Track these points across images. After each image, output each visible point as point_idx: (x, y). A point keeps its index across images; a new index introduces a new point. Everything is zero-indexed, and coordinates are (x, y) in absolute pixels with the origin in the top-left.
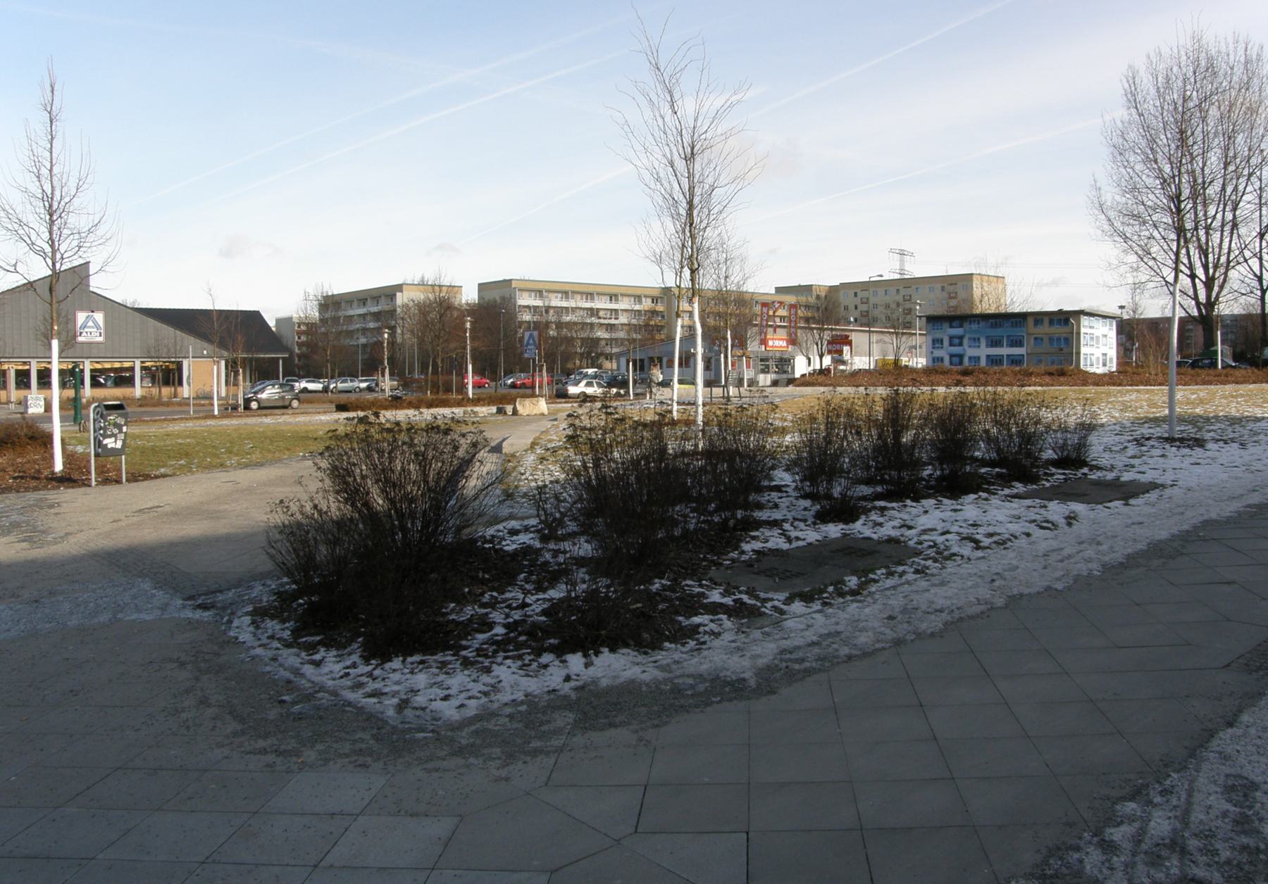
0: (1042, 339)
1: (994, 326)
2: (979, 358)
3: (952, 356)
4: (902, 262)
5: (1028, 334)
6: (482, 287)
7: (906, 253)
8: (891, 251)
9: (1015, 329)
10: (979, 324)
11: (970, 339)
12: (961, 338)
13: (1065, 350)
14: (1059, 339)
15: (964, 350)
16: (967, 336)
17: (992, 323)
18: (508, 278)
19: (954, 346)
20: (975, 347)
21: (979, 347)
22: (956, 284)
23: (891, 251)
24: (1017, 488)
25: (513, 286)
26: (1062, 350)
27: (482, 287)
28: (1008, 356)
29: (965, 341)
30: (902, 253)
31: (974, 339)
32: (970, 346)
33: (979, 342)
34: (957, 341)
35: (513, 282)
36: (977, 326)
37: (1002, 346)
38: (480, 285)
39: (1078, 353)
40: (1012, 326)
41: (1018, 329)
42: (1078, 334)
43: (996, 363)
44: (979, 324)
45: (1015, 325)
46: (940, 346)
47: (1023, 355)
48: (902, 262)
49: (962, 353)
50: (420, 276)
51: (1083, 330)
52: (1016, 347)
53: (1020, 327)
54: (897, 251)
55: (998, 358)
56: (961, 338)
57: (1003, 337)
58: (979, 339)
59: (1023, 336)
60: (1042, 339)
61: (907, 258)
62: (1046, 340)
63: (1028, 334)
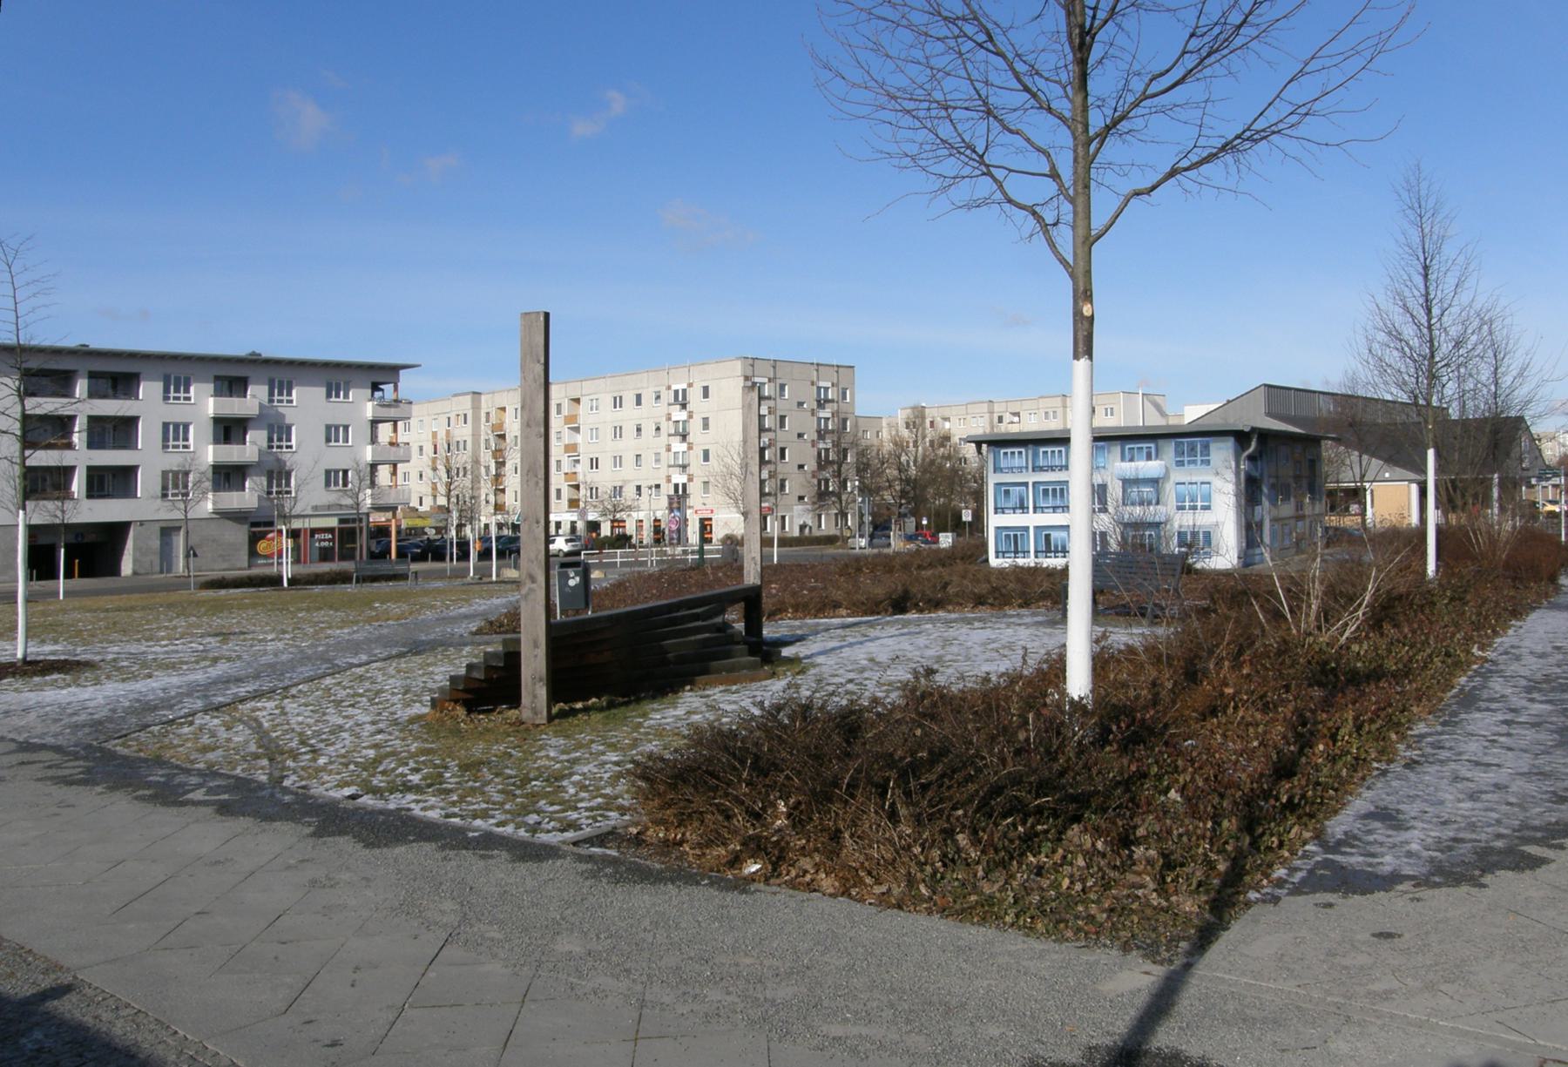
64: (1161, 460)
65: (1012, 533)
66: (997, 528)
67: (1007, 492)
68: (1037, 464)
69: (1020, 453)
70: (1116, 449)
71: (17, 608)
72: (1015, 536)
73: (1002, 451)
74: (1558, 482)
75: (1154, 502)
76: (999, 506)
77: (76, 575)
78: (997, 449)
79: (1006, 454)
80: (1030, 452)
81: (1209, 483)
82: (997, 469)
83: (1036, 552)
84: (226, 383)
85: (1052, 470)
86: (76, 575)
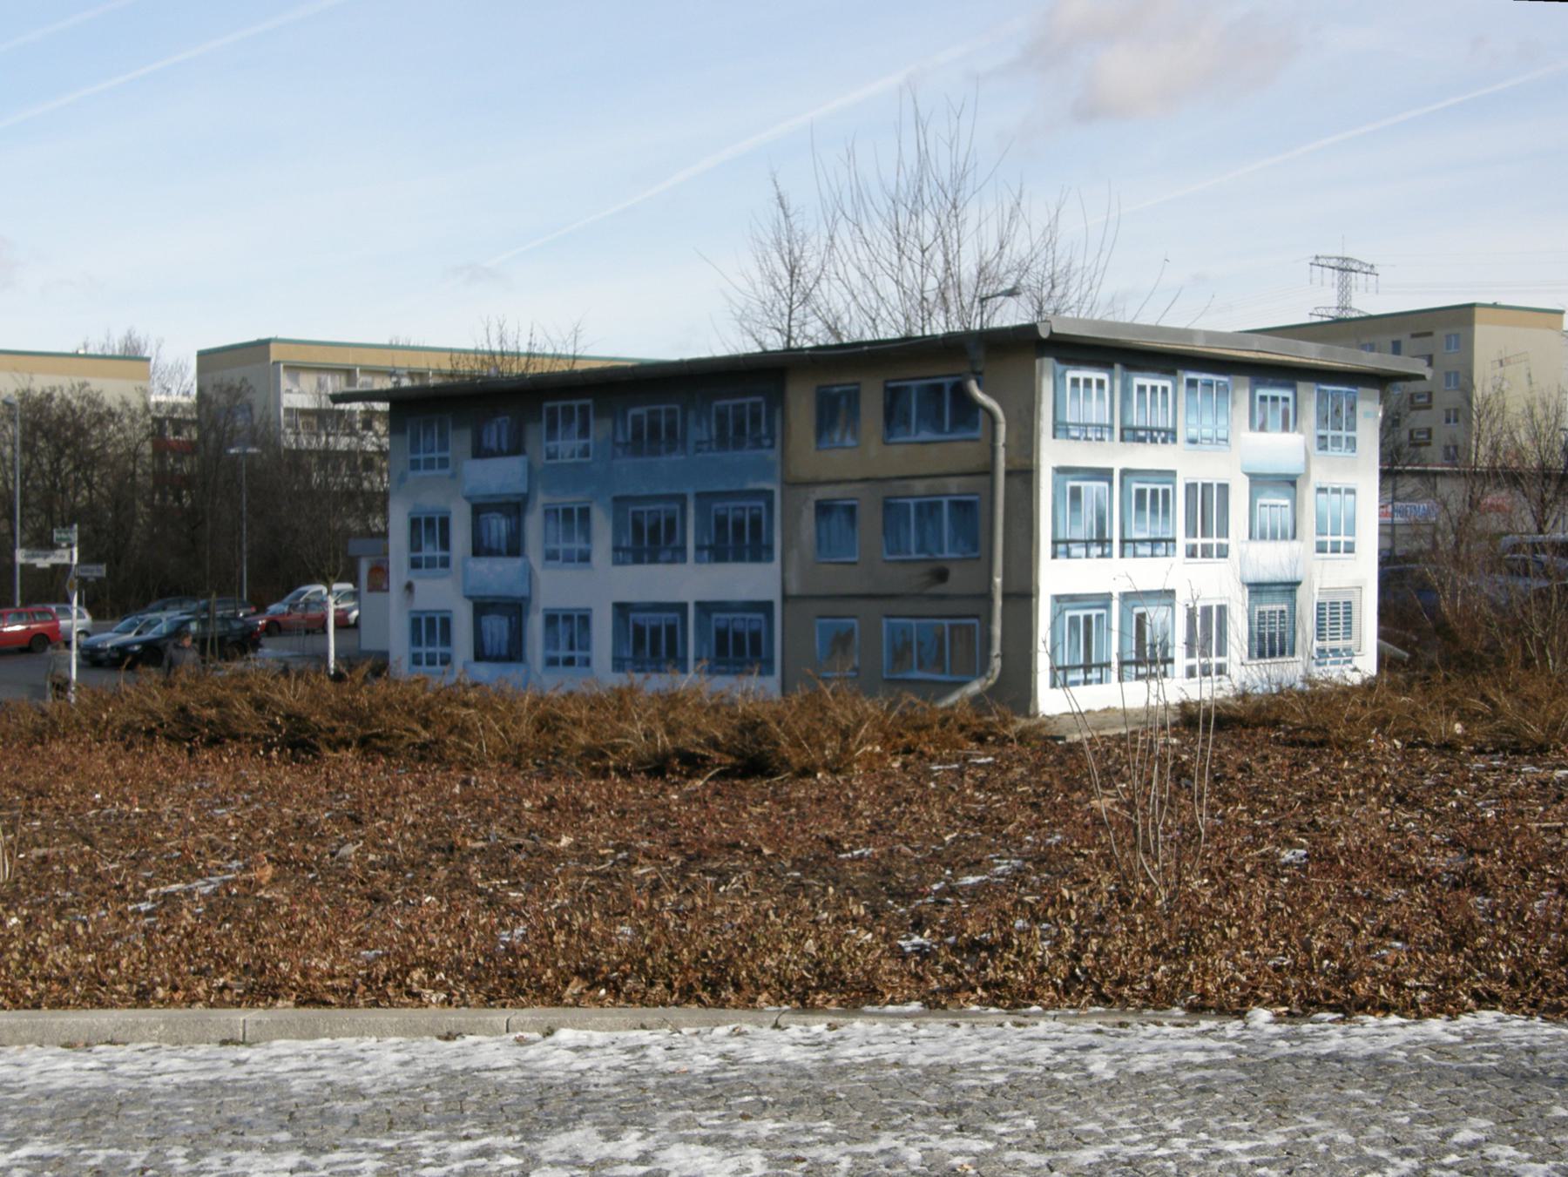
0: (851, 511)
1: (648, 440)
2: (585, 619)
3: (482, 607)
4: (1344, 289)
5: (790, 484)
6: (207, 359)
7: (1355, 267)
8: (1317, 261)
9: (733, 456)
10: (584, 432)
11: (550, 513)
12: (515, 508)
13: (959, 580)
14: (929, 510)
15: (529, 575)
16: (541, 499)
17: (637, 421)
18: (264, 336)
19: (491, 552)
20: (569, 558)
21: (585, 558)
22: (1430, 334)
23: (1317, 261)
24: (1434, 1134)
25: (273, 357)
26: (941, 575)
27: (207, 359)
28: (704, 608)
29: (534, 524)
30: (1345, 268)
31: (568, 513)
32: (551, 556)
33: (587, 535)
34: (498, 526)
35: (272, 346)
36: (578, 443)
37: (678, 555)
38: (203, 356)
39: (1022, 596)
40: (722, 442)
41: (748, 455)
42: (1024, 475)
43: (739, 649)
44: (584, 432)
45: (734, 434)
46: (439, 554)
47: (766, 607)
48: (1344, 289)
49: (519, 591)
50: (125, 333)
51: (1052, 454)
52: (739, 558)
53: (758, 444)
54: (1333, 263)
55: (665, 618)
56: (515, 508)
57: (682, 499)
58: (585, 514)
59: (767, 495)
60: (851, 511)
61: (1357, 279)
62: (870, 520)
63: (792, 484)
64: (1301, 432)
65: (1081, 613)
66: (1058, 599)
67: (1076, 494)
68: (1128, 423)
69: (1100, 384)
70: (1242, 394)
71: (1008, 461)
72: (1088, 619)
73: (1072, 374)
74: (66, 560)
75: (1290, 533)
76: (1061, 536)
77: (1215, 487)
78: (1060, 368)
79: (1075, 382)
80: (1118, 383)
81: (1351, 492)
82: (1060, 428)
83: (1122, 663)
84: (488, 652)
85: (1154, 440)
86: (1215, 487)
